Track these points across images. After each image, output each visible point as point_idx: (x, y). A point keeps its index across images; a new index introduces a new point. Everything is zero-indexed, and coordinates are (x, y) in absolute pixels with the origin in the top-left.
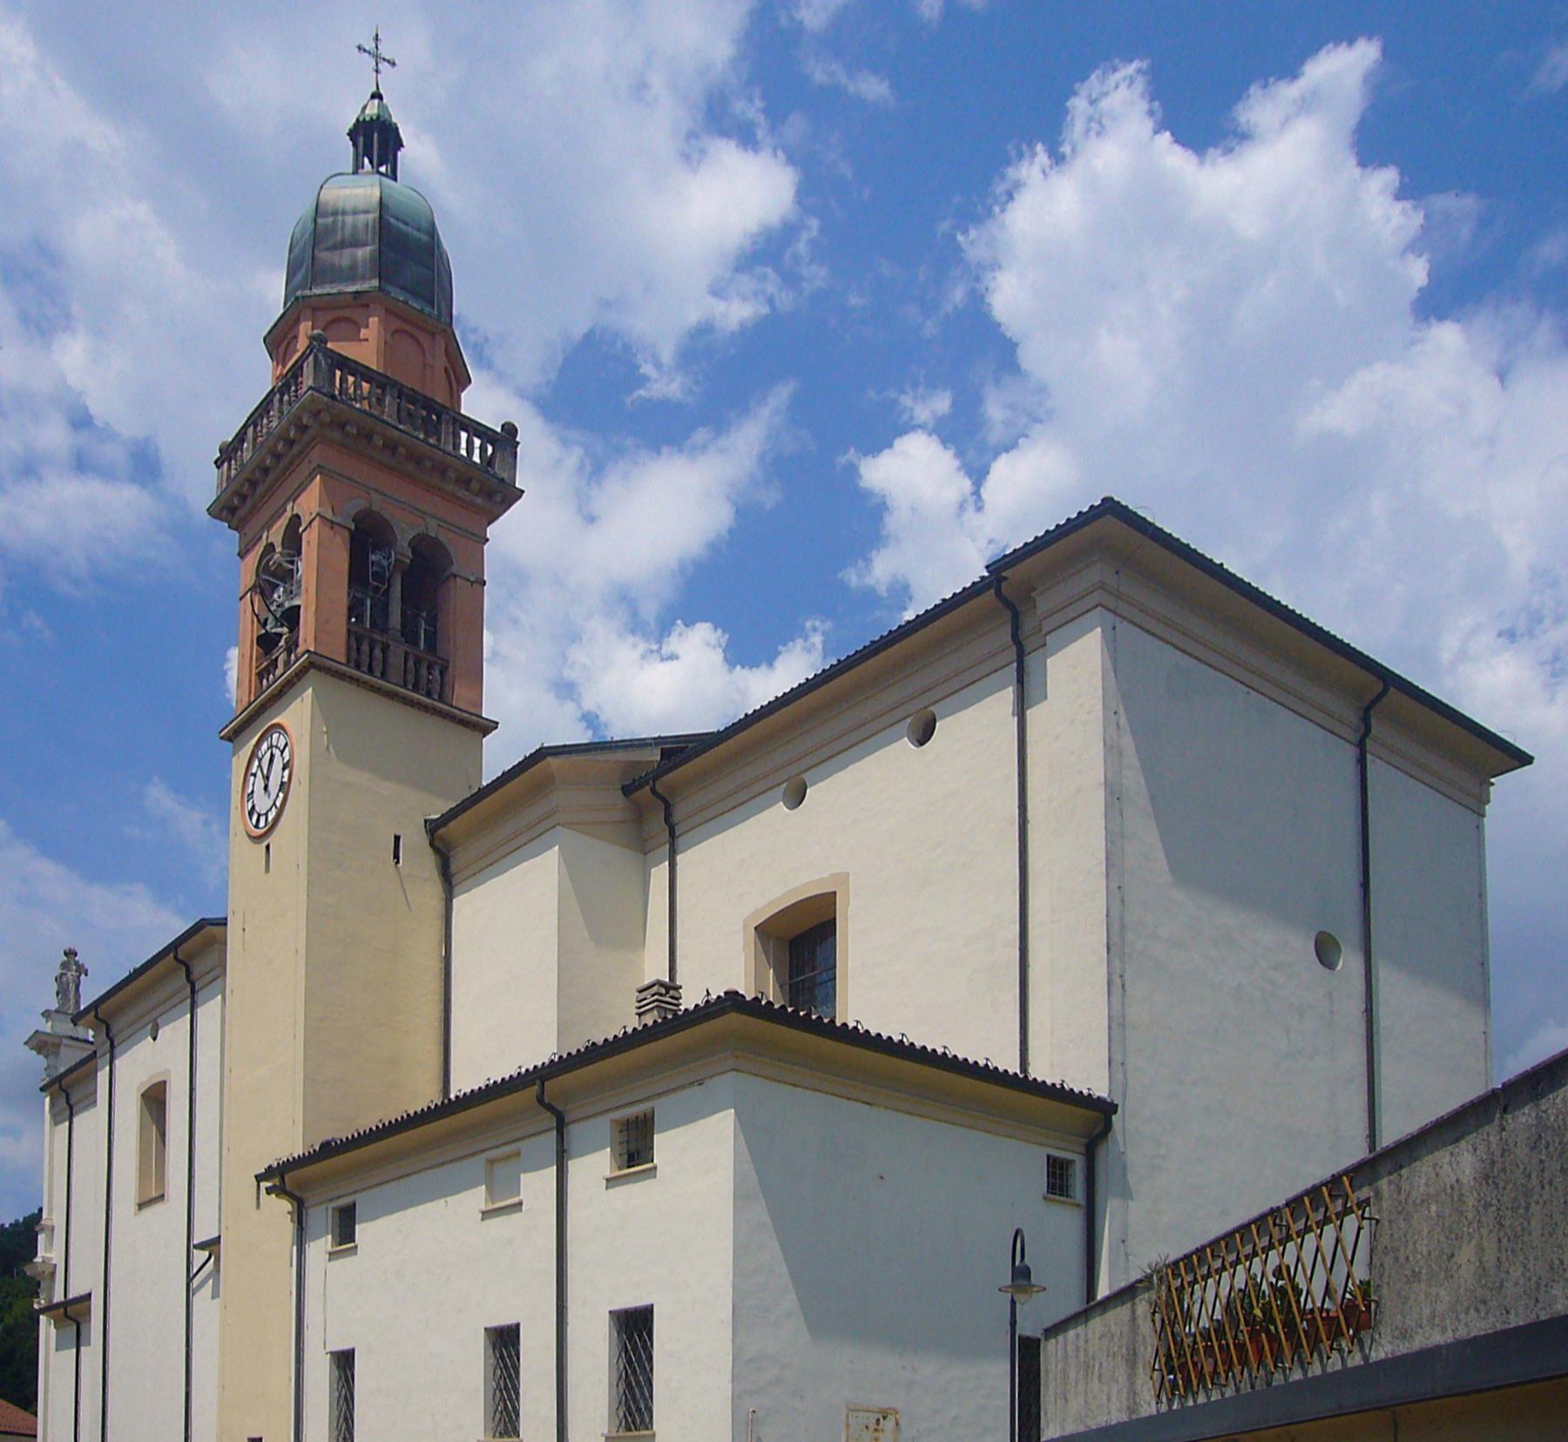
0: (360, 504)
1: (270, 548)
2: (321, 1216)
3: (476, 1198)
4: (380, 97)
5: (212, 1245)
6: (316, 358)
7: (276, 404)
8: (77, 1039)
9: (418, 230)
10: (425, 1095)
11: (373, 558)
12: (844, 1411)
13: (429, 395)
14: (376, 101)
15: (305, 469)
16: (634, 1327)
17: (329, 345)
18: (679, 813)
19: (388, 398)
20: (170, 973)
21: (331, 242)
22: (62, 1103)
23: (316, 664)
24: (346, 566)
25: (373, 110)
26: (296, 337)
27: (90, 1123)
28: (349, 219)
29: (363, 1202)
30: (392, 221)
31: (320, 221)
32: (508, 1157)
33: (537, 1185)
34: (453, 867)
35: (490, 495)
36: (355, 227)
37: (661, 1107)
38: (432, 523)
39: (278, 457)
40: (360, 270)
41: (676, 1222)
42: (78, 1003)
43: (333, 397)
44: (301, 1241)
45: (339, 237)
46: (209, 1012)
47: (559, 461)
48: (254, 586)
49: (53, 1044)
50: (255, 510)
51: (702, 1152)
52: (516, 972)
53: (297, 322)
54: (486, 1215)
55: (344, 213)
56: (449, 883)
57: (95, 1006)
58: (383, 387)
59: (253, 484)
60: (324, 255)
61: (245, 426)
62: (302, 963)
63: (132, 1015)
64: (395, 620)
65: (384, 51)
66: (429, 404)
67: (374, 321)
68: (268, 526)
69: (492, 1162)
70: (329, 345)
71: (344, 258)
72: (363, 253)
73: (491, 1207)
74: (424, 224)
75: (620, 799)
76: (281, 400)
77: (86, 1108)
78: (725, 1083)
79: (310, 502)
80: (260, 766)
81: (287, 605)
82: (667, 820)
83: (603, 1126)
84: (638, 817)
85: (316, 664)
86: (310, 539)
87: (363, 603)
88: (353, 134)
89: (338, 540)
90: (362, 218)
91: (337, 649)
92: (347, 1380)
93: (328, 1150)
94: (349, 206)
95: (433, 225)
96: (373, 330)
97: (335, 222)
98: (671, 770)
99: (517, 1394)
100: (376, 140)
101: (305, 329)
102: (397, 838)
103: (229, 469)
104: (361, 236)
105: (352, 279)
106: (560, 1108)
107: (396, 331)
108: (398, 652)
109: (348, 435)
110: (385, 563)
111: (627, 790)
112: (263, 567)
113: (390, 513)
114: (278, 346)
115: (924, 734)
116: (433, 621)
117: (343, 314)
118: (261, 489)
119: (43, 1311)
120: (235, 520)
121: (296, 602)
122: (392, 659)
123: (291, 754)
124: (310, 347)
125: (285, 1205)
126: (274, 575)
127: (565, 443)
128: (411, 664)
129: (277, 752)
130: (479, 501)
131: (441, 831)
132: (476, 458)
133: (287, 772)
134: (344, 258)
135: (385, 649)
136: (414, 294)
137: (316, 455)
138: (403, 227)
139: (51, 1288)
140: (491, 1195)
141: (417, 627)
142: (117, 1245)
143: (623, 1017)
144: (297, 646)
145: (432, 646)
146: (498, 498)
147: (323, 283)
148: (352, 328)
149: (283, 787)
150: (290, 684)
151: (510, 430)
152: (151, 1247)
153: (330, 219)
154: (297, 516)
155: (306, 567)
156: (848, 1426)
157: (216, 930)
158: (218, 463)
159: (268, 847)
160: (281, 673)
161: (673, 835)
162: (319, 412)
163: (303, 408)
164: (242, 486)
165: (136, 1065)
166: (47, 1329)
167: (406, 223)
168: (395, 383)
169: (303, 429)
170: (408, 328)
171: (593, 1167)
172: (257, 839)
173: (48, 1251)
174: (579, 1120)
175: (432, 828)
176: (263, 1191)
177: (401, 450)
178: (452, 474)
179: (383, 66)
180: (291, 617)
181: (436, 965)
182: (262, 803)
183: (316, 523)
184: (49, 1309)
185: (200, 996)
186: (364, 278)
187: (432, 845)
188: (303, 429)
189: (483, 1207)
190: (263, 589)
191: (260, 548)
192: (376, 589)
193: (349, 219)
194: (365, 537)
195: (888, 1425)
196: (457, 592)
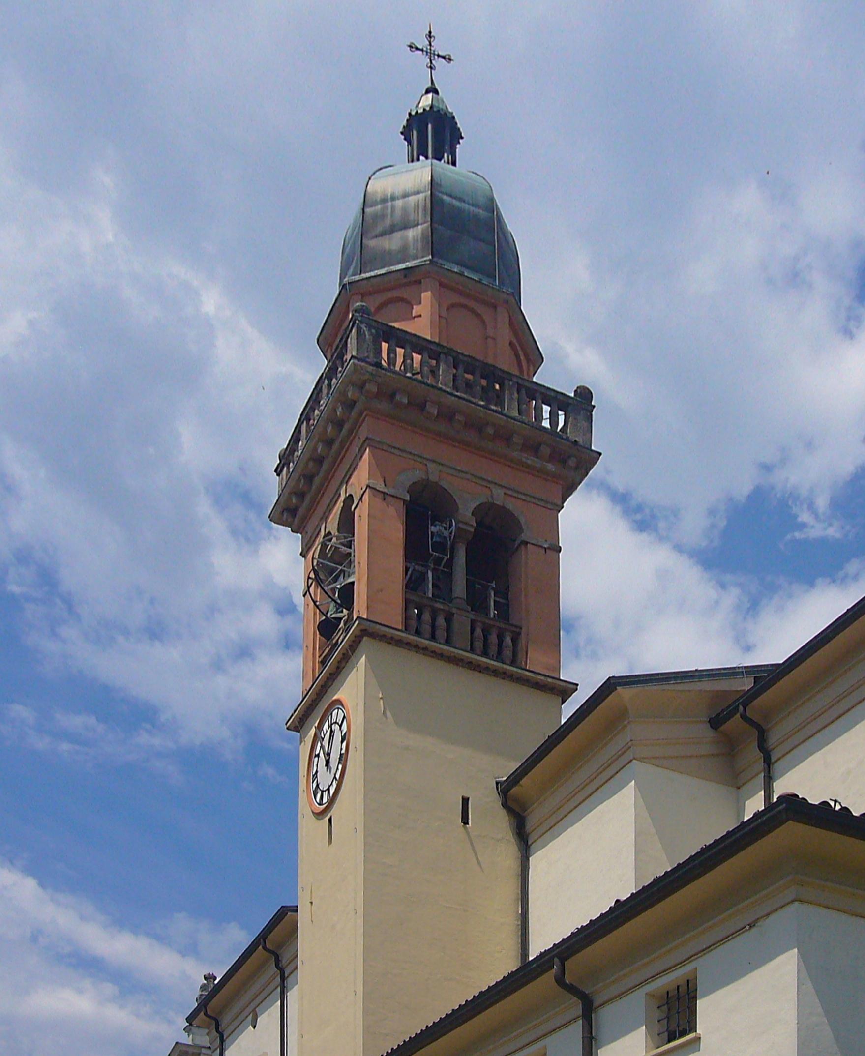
0: (418, 475)
4: (436, 92)
6: (359, 330)
7: (325, 391)
11: (433, 529)
13: (490, 361)
14: (430, 95)
15: (357, 443)
18: (773, 739)
19: (442, 367)
20: (260, 968)
21: (379, 229)
23: (367, 631)
25: (427, 101)
30: (445, 197)
34: (529, 827)
36: (404, 210)
37: (704, 967)
38: (498, 492)
39: (329, 443)
45: (388, 222)
47: (717, 602)
50: (314, 504)
55: (393, 198)
58: (435, 356)
60: (371, 243)
62: (360, 921)
63: (236, 1009)
64: (460, 588)
65: (439, 47)
66: (491, 373)
67: (426, 296)
68: (325, 517)
71: (392, 243)
75: (708, 733)
76: (329, 386)
78: (791, 917)
79: (362, 476)
80: (322, 747)
83: (637, 1002)
85: (367, 631)
88: (406, 133)
89: (392, 511)
90: (412, 199)
91: (393, 616)
94: (398, 192)
100: (433, 132)
102: (465, 801)
107: (453, 306)
108: (462, 621)
110: (446, 533)
111: (715, 723)
113: (452, 484)
116: (504, 592)
118: (317, 481)
121: (350, 580)
122: (456, 625)
126: (331, 560)
127: (723, 586)
128: (478, 631)
129: (336, 727)
130: (550, 467)
131: (514, 791)
133: (344, 744)
134: (392, 243)
135: (449, 619)
138: (456, 203)
141: (486, 599)
145: (504, 611)
146: (572, 462)
149: (343, 759)
151: (584, 395)
153: (379, 207)
154: (351, 495)
161: (768, 763)
167: (461, 200)
168: (449, 352)
169: (350, 405)
170: (463, 300)
172: (319, 815)
174: (610, 1000)
175: (505, 789)
179: (439, 63)
183: (366, 496)
187: (505, 805)
188: (350, 405)
192: (438, 561)
193: (399, 203)
194: (422, 511)
196: (528, 561)
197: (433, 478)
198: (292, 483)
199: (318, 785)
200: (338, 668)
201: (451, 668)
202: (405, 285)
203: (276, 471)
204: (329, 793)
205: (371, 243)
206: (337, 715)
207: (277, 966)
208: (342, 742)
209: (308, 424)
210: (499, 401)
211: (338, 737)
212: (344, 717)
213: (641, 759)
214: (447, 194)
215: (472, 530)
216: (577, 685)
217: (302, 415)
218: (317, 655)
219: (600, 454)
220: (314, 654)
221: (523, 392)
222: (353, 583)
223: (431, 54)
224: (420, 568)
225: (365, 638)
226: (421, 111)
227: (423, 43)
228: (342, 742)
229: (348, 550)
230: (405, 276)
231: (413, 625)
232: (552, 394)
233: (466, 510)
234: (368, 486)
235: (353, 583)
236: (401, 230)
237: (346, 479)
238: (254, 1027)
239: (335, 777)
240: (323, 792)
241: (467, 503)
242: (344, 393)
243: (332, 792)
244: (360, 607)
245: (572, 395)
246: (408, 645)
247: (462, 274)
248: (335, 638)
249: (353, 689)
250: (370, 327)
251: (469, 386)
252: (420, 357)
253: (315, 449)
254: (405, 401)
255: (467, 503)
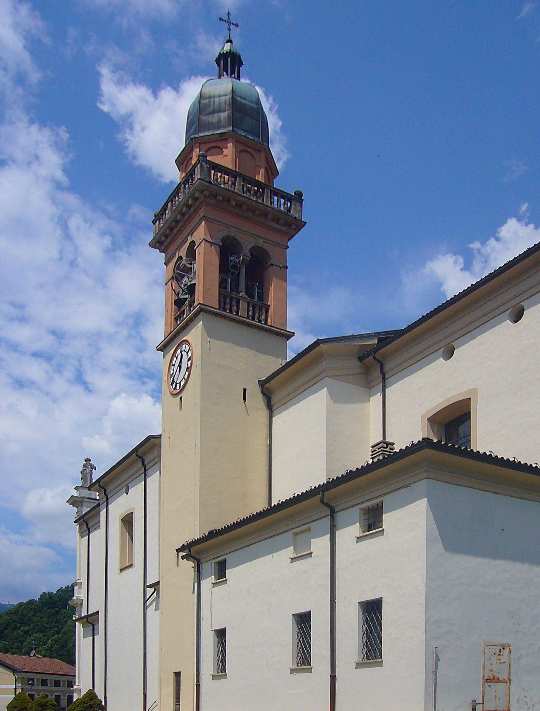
0: (223, 234)
1: (181, 258)
2: (209, 567)
3: (289, 552)
5: (156, 585)
6: (201, 165)
7: (182, 190)
8: (91, 499)
9: (251, 102)
10: (260, 506)
11: (231, 258)
12: (483, 645)
14: (229, 44)
15: (197, 218)
16: (372, 610)
17: (208, 158)
21: (207, 113)
22: (85, 528)
23: (203, 310)
24: (218, 263)
25: (227, 47)
26: (191, 158)
27: (97, 536)
28: (217, 100)
29: (230, 558)
30: (238, 98)
31: (202, 101)
32: (303, 532)
33: (320, 545)
34: (273, 402)
35: (288, 224)
36: (219, 103)
38: (261, 241)
40: (223, 123)
41: (399, 554)
42: (91, 479)
43: (211, 183)
44: (199, 580)
45: (212, 108)
46: (153, 480)
48: (173, 277)
49: (80, 501)
51: (409, 521)
52: (310, 441)
53: (192, 150)
54: (293, 560)
55: (214, 97)
56: (271, 409)
57: (99, 480)
59: (172, 229)
60: (204, 118)
61: (167, 203)
63: (116, 484)
67: (230, 145)
69: (296, 534)
70: (208, 158)
71: (214, 119)
72: (224, 115)
73: (295, 556)
74: (254, 100)
75: (357, 363)
76: (185, 187)
77: (96, 529)
78: (423, 485)
79: (200, 234)
81: (189, 284)
82: (382, 371)
83: (355, 512)
84: (367, 371)
85: (203, 310)
86: (200, 252)
87: (226, 282)
88: (218, 61)
90: (223, 98)
91: (214, 302)
92: (222, 643)
93: (212, 534)
94: (217, 93)
95: (259, 99)
96: (229, 149)
97: (210, 102)
98: (383, 347)
99: (310, 646)
101: (196, 152)
102: (245, 390)
103: (160, 223)
104: (223, 106)
105: (219, 128)
106: (332, 505)
109: (219, 201)
110: (237, 261)
112: (177, 267)
113: (240, 237)
114: (182, 164)
115: (517, 316)
116: (261, 287)
117: (216, 144)
118: (175, 231)
119: (77, 620)
120: (163, 247)
121: (193, 282)
123: (192, 354)
124: (199, 160)
125: (191, 564)
129: (184, 353)
130: (283, 228)
131: (267, 385)
132: (282, 208)
133: (190, 362)
134: (214, 119)
135: (238, 302)
136: (251, 134)
137: (202, 213)
138: (244, 101)
139: (81, 611)
140: (295, 550)
141: (253, 291)
142: (113, 593)
143: (365, 458)
144: (194, 302)
146: (294, 227)
147: (204, 131)
148: (219, 150)
149: (188, 369)
150: (191, 320)
152: (127, 588)
153: (207, 100)
155: (198, 266)
156: (485, 653)
157: (156, 440)
158: (154, 222)
159: (181, 398)
160: (186, 317)
161: (384, 379)
162: (204, 190)
163: (196, 189)
164: (166, 230)
165: (118, 507)
166: (79, 628)
167: (245, 99)
168: (240, 175)
171: (349, 533)
173: (79, 594)
175: (262, 384)
176: (180, 558)
177: (244, 206)
178: (270, 216)
180: (191, 289)
181: (266, 449)
182: (180, 378)
183: (202, 244)
184: (79, 619)
185: (148, 472)
186: (224, 127)
187: (262, 392)
188: (196, 199)
189: (292, 556)
190: (177, 277)
191: (175, 259)
193: (217, 100)
194: (227, 249)
195: (506, 652)
197: (232, 234)
198: (163, 230)
199: (173, 380)
200: (186, 324)
201: (238, 326)
202: (220, 140)
203: (153, 222)
204: (180, 385)
205: (204, 118)
206: (185, 347)
207: (143, 464)
208: (188, 361)
209: (172, 203)
210: (262, 195)
211: (185, 359)
212: (189, 349)
213: (330, 377)
214: (239, 97)
215: (249, 259)
216: (294, 333)
217: (169, 198)
218: (173, 315)
219: (306, 223)
220: (171, 314)
221: (272, 193)
222: (195, 284)
223: (229, 23)
224: (225, 277)
225: (201, 313)
226: (225, 52)
227: (225, 18)
228: (188, 361)
229: (190, 266)
230: (220, 137)
231: (222, 305)
232: (285, 195)
233: (246, 249)
234: (204, 239)
235: (195, 284)
236: (217, 112)
237: (192, 233)
238: (127, 494)
239: (184, 378)
240: (176, 384)
241: (247, 245)
242: (193, 194)
243: (182, 384)
244: (199, 297)
245: (293, 194)
246: (221, 316)
247: (246, 137)
248: (183, 308)
249: (195, 335)
250: (205, 163)
251: (249, 190)
252: (228, 177)
253: (176, 217)
254: (221, 199)
255: (247, 245)
